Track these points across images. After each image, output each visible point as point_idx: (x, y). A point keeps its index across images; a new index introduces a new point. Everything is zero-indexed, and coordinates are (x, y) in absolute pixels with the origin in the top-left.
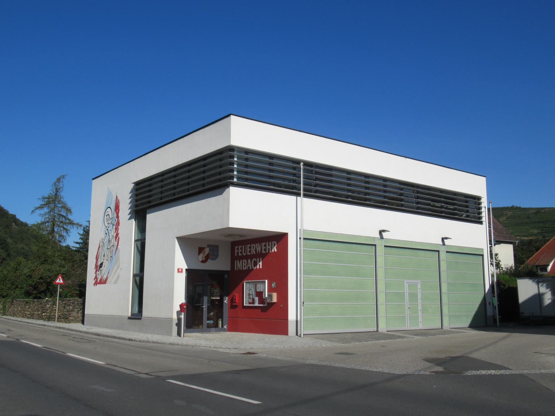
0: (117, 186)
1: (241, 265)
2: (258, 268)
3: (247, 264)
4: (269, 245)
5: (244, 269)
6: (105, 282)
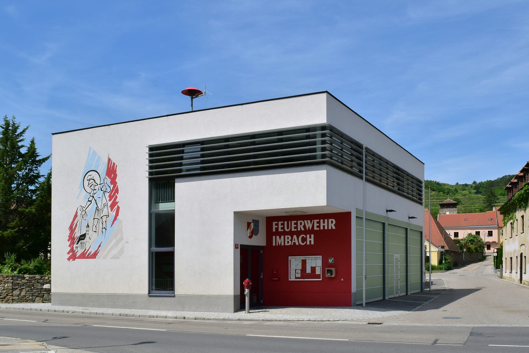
0: (131, 151)
1: (279, 241)
2: (308, 243)
3: (291, 240)
4: (324, 222)
5: (286, 244)
6: (94, 256)
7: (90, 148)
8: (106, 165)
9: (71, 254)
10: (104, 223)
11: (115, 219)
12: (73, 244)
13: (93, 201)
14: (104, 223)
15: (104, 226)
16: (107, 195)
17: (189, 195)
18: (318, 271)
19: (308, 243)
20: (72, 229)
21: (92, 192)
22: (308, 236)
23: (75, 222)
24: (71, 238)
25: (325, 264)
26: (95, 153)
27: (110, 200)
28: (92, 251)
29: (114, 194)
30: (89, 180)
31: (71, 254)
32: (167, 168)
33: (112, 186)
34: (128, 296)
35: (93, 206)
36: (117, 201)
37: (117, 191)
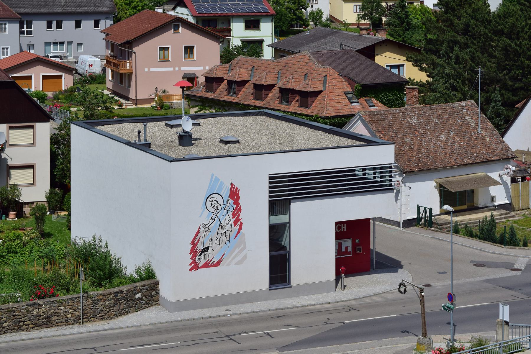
2: (342, 230)
6: (218, 264)
7: (213, 175)
8: (229, 189)
9: (193, 265)
10: (228, 237)
11: (239, 232)
12: (196, 257)
13: (216, 219)
14: (228, 237)
15: (228, 239)
16: (230, 213)
17: (301, 211)
18: (350, 249)
19: (342, 230)
20: (194, 244)
21: (215, 212)
22: (342, 225)
23: (198, 237)
24: (194, 252)
25: (354, 245)
26: (217, 179)
27: (233, 218)
28: (216, 260)
29: (237, 212)
30: (212, 201)
31: (193, 265)
32: (285, 192)
33: (235, 206)
34: (250, 293)
35: (217, 223)
36: (240, 218)
37: (240, 210)
